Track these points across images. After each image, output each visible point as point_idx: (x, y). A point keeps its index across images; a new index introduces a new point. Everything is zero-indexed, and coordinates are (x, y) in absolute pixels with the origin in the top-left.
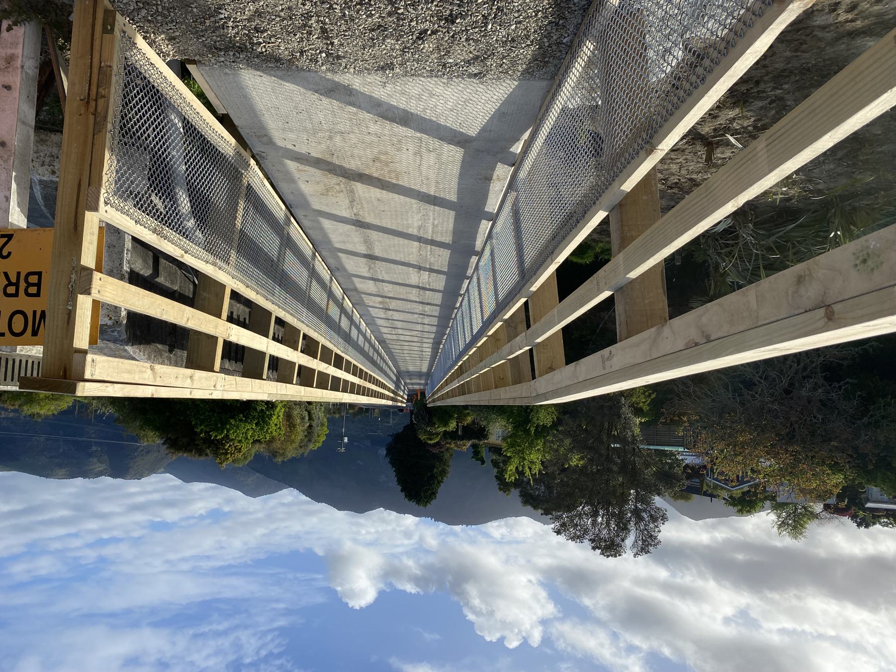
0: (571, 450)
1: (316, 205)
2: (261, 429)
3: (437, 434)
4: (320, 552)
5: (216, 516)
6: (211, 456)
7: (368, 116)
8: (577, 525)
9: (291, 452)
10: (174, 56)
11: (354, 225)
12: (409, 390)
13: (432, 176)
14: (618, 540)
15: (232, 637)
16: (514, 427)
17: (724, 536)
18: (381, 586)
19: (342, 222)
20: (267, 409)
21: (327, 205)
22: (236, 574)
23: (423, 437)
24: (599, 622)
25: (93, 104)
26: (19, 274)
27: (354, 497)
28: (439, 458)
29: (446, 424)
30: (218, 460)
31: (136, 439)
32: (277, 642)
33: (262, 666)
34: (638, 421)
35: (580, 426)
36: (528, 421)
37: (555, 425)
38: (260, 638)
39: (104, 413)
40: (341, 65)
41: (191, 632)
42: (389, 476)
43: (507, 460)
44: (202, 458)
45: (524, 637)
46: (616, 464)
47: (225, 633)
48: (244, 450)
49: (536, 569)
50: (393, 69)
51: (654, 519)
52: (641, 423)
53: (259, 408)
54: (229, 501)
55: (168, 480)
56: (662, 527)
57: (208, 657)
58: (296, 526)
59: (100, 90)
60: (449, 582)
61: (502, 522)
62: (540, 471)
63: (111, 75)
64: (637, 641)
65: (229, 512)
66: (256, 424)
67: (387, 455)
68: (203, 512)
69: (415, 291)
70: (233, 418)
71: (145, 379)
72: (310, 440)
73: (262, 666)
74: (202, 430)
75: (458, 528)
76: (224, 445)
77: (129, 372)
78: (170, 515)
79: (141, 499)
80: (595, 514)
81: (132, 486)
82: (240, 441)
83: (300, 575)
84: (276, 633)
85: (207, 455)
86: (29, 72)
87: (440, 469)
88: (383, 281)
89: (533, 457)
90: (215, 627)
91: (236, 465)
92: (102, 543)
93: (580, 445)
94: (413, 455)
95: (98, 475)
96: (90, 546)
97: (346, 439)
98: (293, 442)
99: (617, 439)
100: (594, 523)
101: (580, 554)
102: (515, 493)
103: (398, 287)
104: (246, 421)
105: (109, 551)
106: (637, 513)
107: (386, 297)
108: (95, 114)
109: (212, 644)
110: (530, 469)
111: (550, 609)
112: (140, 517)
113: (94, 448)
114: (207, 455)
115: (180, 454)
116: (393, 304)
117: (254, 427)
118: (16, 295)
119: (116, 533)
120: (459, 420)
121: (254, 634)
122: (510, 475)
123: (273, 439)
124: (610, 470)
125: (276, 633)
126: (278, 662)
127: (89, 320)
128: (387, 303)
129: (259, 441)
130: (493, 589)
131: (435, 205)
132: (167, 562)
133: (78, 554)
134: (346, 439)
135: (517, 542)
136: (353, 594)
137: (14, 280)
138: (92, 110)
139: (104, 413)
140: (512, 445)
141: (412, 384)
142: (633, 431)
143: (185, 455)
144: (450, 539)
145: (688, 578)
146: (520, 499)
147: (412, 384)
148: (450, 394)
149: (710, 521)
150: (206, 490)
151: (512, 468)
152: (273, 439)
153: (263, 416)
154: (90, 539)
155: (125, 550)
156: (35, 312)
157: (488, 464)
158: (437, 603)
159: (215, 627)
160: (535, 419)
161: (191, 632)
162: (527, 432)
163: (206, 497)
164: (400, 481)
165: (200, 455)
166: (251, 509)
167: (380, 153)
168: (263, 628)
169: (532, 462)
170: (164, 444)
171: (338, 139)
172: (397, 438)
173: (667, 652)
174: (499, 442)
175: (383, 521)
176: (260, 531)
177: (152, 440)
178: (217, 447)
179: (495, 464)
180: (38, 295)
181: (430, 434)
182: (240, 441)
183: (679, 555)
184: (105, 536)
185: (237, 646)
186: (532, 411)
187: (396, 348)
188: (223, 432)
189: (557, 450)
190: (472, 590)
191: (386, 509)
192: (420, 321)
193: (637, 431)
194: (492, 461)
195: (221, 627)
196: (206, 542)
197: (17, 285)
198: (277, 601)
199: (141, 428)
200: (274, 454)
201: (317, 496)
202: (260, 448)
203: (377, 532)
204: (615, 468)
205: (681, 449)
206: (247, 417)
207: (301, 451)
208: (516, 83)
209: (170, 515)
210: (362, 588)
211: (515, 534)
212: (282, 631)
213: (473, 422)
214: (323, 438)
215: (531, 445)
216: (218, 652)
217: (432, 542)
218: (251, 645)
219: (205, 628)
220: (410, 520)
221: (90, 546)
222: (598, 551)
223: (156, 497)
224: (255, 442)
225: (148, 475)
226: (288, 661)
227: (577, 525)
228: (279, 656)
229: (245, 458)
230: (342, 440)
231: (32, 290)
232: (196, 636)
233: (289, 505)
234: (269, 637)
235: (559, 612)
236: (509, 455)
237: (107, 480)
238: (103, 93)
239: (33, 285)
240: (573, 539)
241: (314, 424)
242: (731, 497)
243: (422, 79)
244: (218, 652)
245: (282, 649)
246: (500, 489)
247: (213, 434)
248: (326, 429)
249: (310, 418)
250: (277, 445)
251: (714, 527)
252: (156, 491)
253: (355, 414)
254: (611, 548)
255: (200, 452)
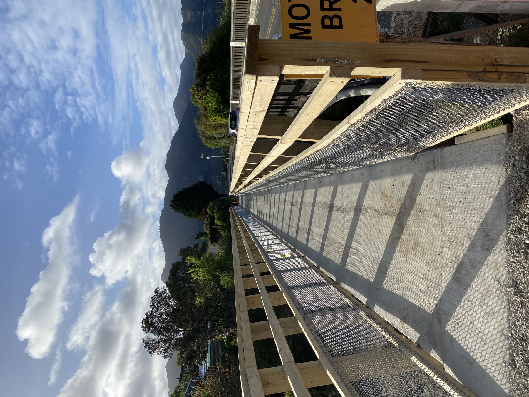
0: (205, 298)
1: (373, 185)
2: (213, 110)
3: (213, 213)
4: (142, 144)
5: (162, 82)
6: (196, 82)
7: (461, 253)
8: (160, 303)
9: (200, 128)
10: (517, 118)
11: (357, 206)
12: (238, 197)
13: (403, 279)
14: (152, 329)
15: (91, 91)
16: (218, 261)
17: (157, 387)
18: (124, 182)
19: (359, 198)
20: (225, 114)
21: (373, 192)
22: (128, 94)
23: (211, 204)
24: (102, 317)
25: (493, 69)
26: (340, 10)
27: (175, 162)
28: (199, 213)
29: (219, 219)
30: (194, 86)
31: (205, 36)
32: (89, 117)
33: (75, 109)
34: (225, 338)
35: (220, 302)
36: (222, 270)
37: (220, 287)
38: (91, 107)
39: (219, 19)
40: (519, 253)
41: (94, 68)
42: (188, 183)
43: (199, 258)
44: (195, 77)
45: (94, 264)
46: (198, 326)
47: (94, 87)
48: (200, 101)
49: (134, 275)
50: (515, 295)
51: (166, 350)
52: (223, 340)
53: (225, 109)
54: (170, 89)
55: (182, 56)
56: (160, 356)
57: (80, 78)
58: (157, 128)
59: (505, 75)
60: (126, 222)
61: (162, 248)
62: (192, 278)
63: (518, 82)
64: (92, 341)
65: (164, 89)
66: (216, 108)
67: (200, 182)
68: (164, 74)
69: (307, 226)
70: (219, 94)
71: (254, 107)
72: (207, 138)
73: (75, 109)
74: (211, 76)
75: (158, 223)
76: (203, 89)
77: (261, 100)
78: (161, 55)
79: (170, 39)
80: (167, 314)
81: (177, 34)
82: (205, 99)
83: (128, 131)
84: (94, 116)
85: (197, 80)
86: (500, 7)
87: (192, 214)
88: (313, 209)
89: (201, 273)
90: (97, 81)
91: (191, 96)
92: (145, 19)
93: (209, 303)
94: (200, 196)
95: (184, 16)
96: (143, 11)
97: (208, 158)
98: (206, 129)
99: (213, 326)
100: (162, 313)
101: (143, 307)
102: (179, 259)
103: (309, 216)
104: (217, 102)
105: (140, 22)
106: (168, 340)
107: (301, 206)
108: (484, 71)
109: (87, 80)
110: (194, 272)
111: (110, 281)
112: (160, 39)
113: (199, 13)
114: (197, 80)
115: (197, 64)
116: (296, 209)
117: (214, 107)
118: (323, 9)
119: (150, 26)
120: (222, 227)
121: (93, 104)
122: (190, 260)
123: (207, 117)
124: (194, 322)
125: (94, 116)
126: (77, 118)
127: (306, 73)
128: (297, 205)
129: (206, 109)
130: (122, 249)
131: (378, 270)
132: (135, 55)
133: (138, 5)
134: (208, 158)
135: (150, 258)
136: (119, 163)
137: (335, 6)
138: (488, 69)
139: (219, 19)
140: (207, 260)
141: (242, 199)
142: (218, 335)
143: (196, 67)
144: (151, 220)
145: (131, 365)
146: (176, 262)
147: (242, 199)
148: (239, 234)
149: (166, 376)
150: (177, 76)
151: (194, 261)
152: (207, 117)
153: (220, 112)
154: (147, 11)
155: (141, 31)
156: (309, 25)
157: (196, 242)
158: (111, 217)
159: (97, 81)
160: (223, 274)
161: (94, 68)
162: (216, 270)
163: (173, 77)
164: (184, 190)
165: (197, 76)
166: (166, 102)
167: (424, 249)
168: (97, 108)
169: (197, 273)
170: (203, 55)
171: (436, 221)
172: (210, 187)
173: (86, 358)
174: (209, 251)
175: (161, 179)
176: (154, 108)
177: (205, 47)
178: (201, 85)
179: (196, 246)
180: (324, 26)
181: (213, 209)
182: (205, 99)
183: (145, 364)
184: (149, 20)
185: (86, 94)
186: (228, 272)
187: (265, 198)
188: (210, 89)
189: (205, 288)
190: (122, 237)
191: (168, 181)
192: (285, 221)
193: (218, 338)
194: (198, 244)
195: (97, 85)
196: (146, 76)
197: (331, 9)
198: (113, 117)
199: (211, 41)
200: (198, 118)
201: (174, 141)
202: (202, 110)
203: (155, 175)
204: (195, 326)
205: (208, 364)
206: (220, 102)
207: (201, 133)
208: (507, 391)
209: (161, 55)
210: (123, 169)
211: (155, 256)
212: (95, 120)
213: (221, 235)
214: (208, 146)
215: (208, 272)
216: (83, 83)
217: (149, 210)
218: (87, 102)
219: (96, 76)
220: (162, 194)
221: (143, 11)
222: (145, 317)
223: (172, 48)
224: (205, 107)
225: (184, 44)
226: (78, 123)
227: (160, 303)
228: (81, 118)
229: (196, 102)
230: (208, 156)
231: (327, 22)
232: (92, 71)
233: (169, 124)
234: (91, 112)
235: (109, 287)
236: (202, 258)
237: (181, 21)
238: (503, 77)
239: (331, 22)
240: (152, 300)
241: (217, 140)
242: (180, 392)
243: (506, 314)
244: (83, 83)
245: (85, 120)
246: (181, 250)
247: (209, 83)
248: (214, 147)
249: (220, 138)
250: (204, 120)
251: (162, 379)
252: (175, 47)
253: (223, 162)
254: (147, 325)
255: (198, 76)
